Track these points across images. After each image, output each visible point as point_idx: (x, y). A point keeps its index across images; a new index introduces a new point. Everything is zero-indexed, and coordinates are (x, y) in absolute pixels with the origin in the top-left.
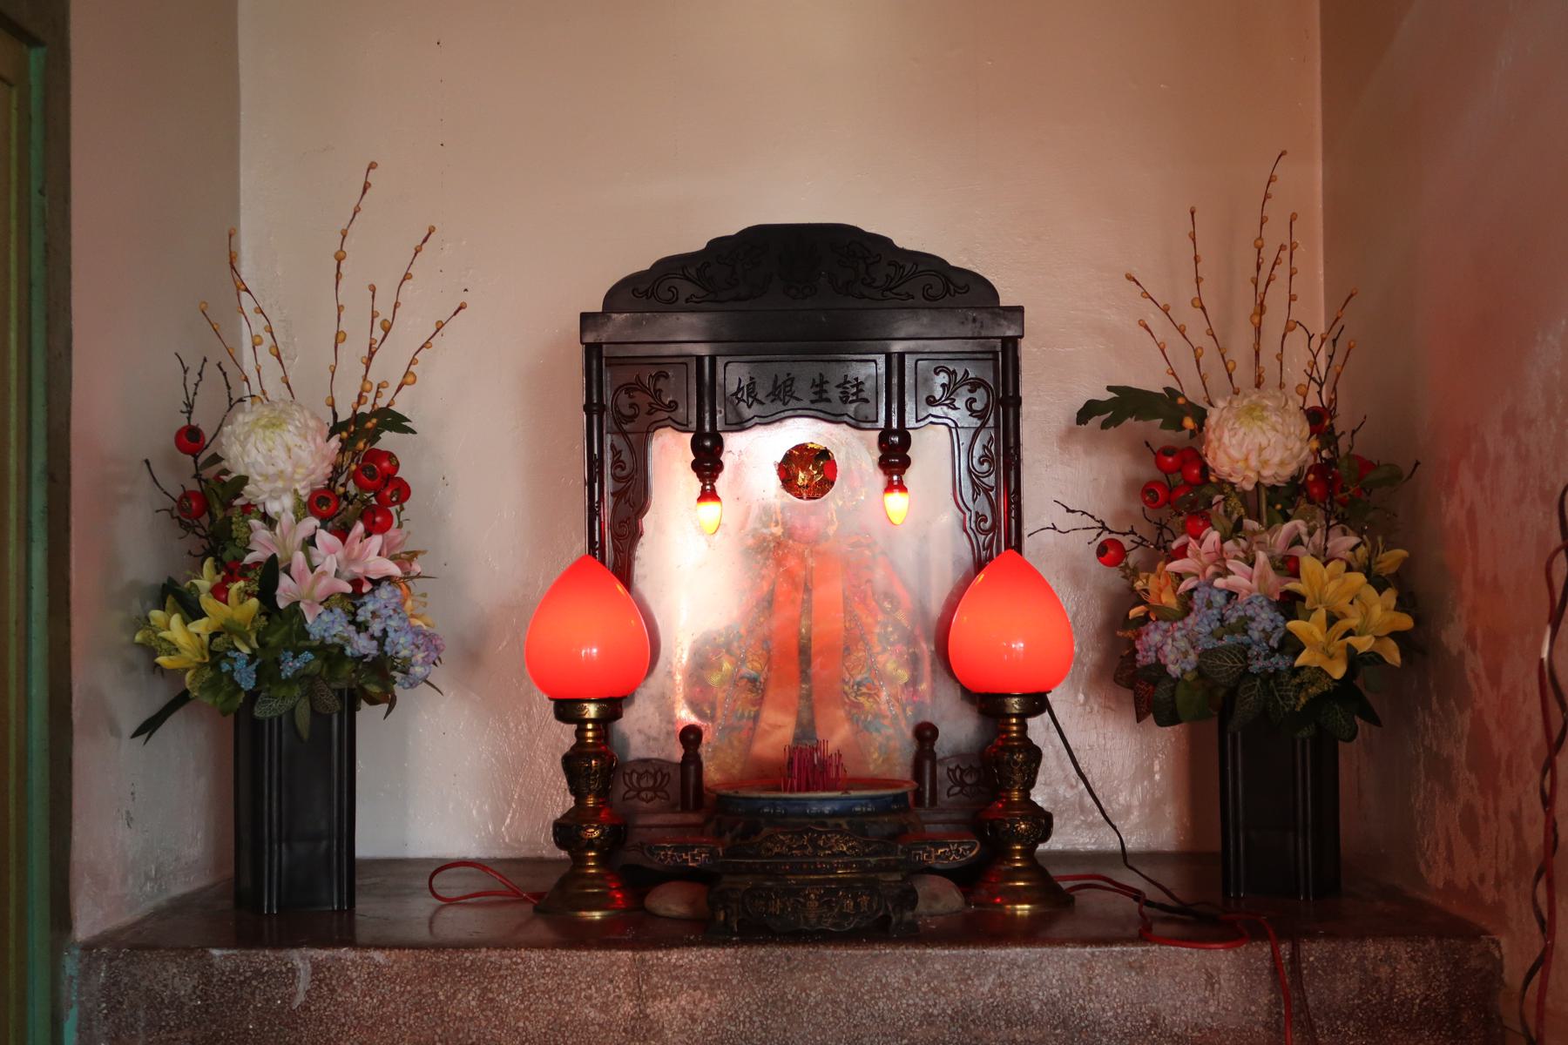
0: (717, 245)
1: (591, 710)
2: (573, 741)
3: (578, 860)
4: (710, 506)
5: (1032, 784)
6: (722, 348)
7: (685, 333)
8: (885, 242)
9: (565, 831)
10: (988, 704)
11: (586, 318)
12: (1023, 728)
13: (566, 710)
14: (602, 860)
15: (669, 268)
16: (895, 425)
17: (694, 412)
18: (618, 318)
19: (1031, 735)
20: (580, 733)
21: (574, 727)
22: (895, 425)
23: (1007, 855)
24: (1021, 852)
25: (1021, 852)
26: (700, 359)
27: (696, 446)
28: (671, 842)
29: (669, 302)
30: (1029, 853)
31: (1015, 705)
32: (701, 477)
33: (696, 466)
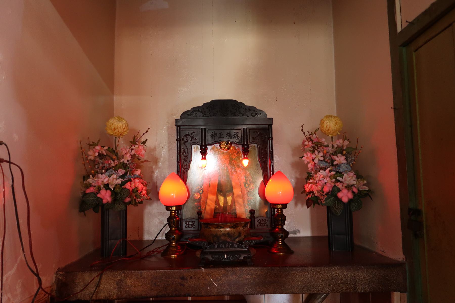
0: (205, 104)
1: (174, 208)
2: (169, 215)
3: (171, 243)
4: (204, 160)
5: (284, 224)
6: (208, 127)
7: (200, 123)
8: (243, 104)
9: (168, 235)
10: (273, 206)
11: (177, 120)
12: (282, 211)
13: (168, 208)
14: (176, 243)
15: (195, 109)
16: (204, 144)
17: (201, 140)
18: (183, 120)
19: (283, 213)
20: (171, 213)
21: (170, 212)
22: (204, 144)
23: (278, 241)
24: (281, 240)
25: (281, 240)
26: (244, 128)
27: (201, 148)
28: (204, 235)
29: (195, 117)
30: (283, 241)
31: (280, 206)
32: (202, 155)
33: (201, 152)
